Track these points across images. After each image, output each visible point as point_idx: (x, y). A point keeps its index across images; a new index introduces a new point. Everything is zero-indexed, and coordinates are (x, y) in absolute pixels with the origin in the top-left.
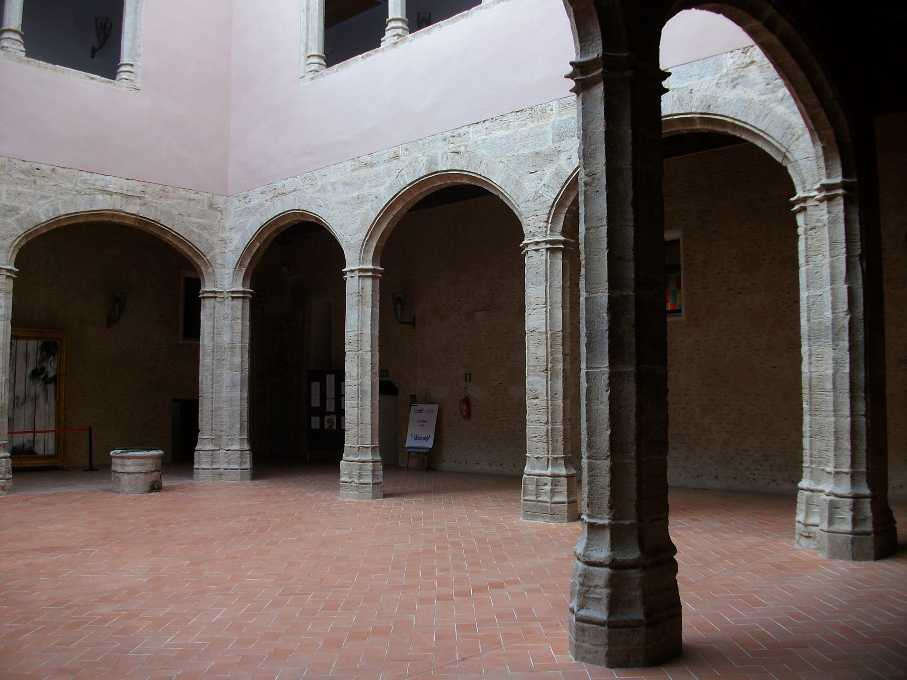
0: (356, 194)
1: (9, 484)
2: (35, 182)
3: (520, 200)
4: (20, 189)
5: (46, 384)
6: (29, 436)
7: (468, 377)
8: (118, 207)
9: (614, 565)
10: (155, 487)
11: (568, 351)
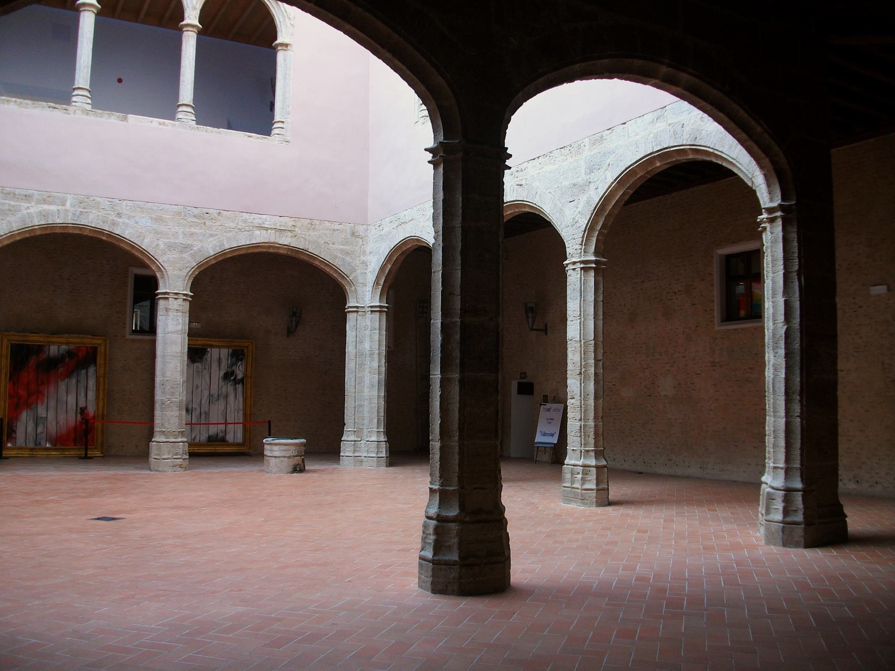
1: (187, 462)
2: (205, 224)
3: (563, 226)
4: (193, 230)
5: (236, 384)
6: (222, 427)
8: (272, 240)
10: (298, 469)
11: (600, 357)
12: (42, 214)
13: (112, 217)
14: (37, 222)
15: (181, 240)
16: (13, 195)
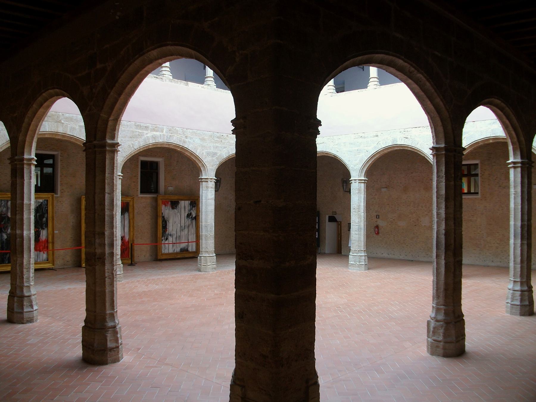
0: (357, 148)
4: (217, 144)
7: (378, 217)
12: (154, 137)
13: (184, 138)
14: (151, 141)
15: (212, 150)
16: (138, 126)
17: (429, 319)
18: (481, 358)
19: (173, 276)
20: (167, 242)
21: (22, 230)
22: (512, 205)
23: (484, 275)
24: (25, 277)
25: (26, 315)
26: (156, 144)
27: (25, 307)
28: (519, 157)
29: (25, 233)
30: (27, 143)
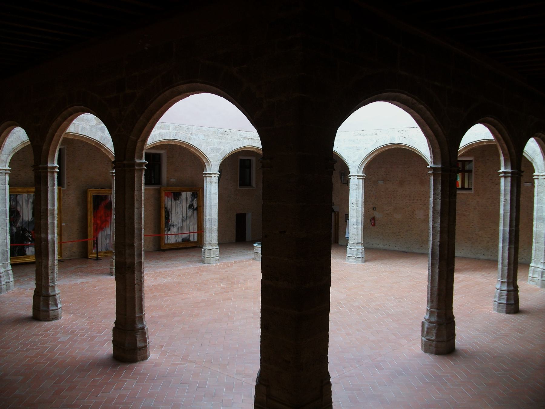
4: (220, 140)
7: (374, 209)
9: (508, 291)
13: (189, 135)
17: (424, 320)
18: (468, 356)
19: (179, 268)
20: (169, 233)
21: (47, 234)
22: (502, 212)
23: (476, 269)
24: (50, 277)
25: (51, 313)
26: (163, 141)
27: (50, 306)
28: (510, 167)
29: (50, 237)
30: (50, 152)
